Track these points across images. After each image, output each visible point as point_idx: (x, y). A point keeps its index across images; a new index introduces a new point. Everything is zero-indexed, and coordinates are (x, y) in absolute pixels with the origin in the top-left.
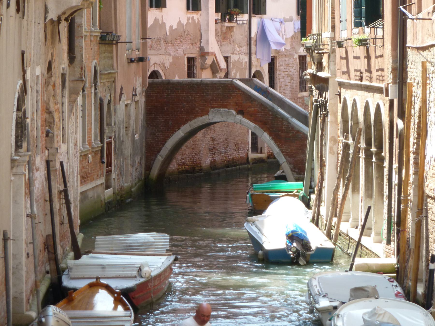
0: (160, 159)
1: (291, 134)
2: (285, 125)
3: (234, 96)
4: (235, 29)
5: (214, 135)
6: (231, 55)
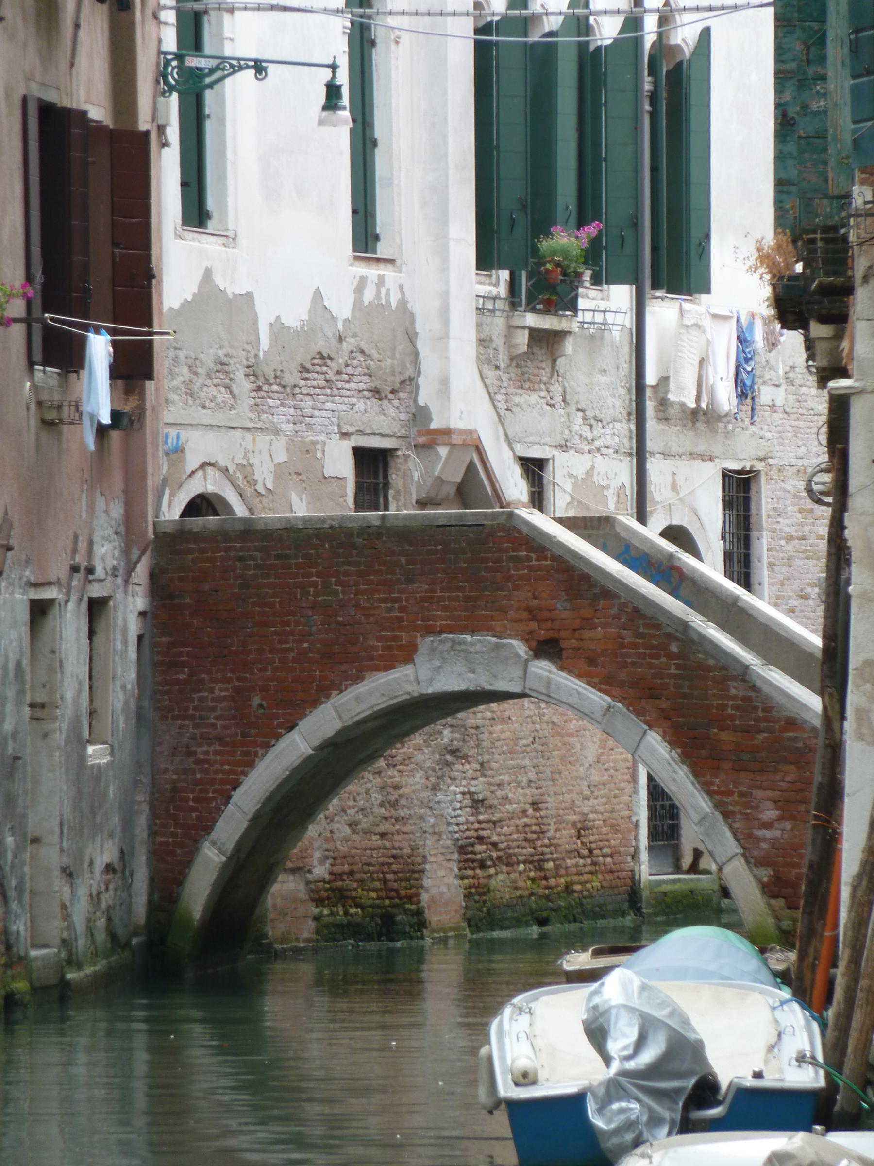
0: (211, 859)
1: (761, 737)
2: (735, 698)
3: (520, 578)
4: (569, 346)
5: (479, 787)
6: (556, 452)
